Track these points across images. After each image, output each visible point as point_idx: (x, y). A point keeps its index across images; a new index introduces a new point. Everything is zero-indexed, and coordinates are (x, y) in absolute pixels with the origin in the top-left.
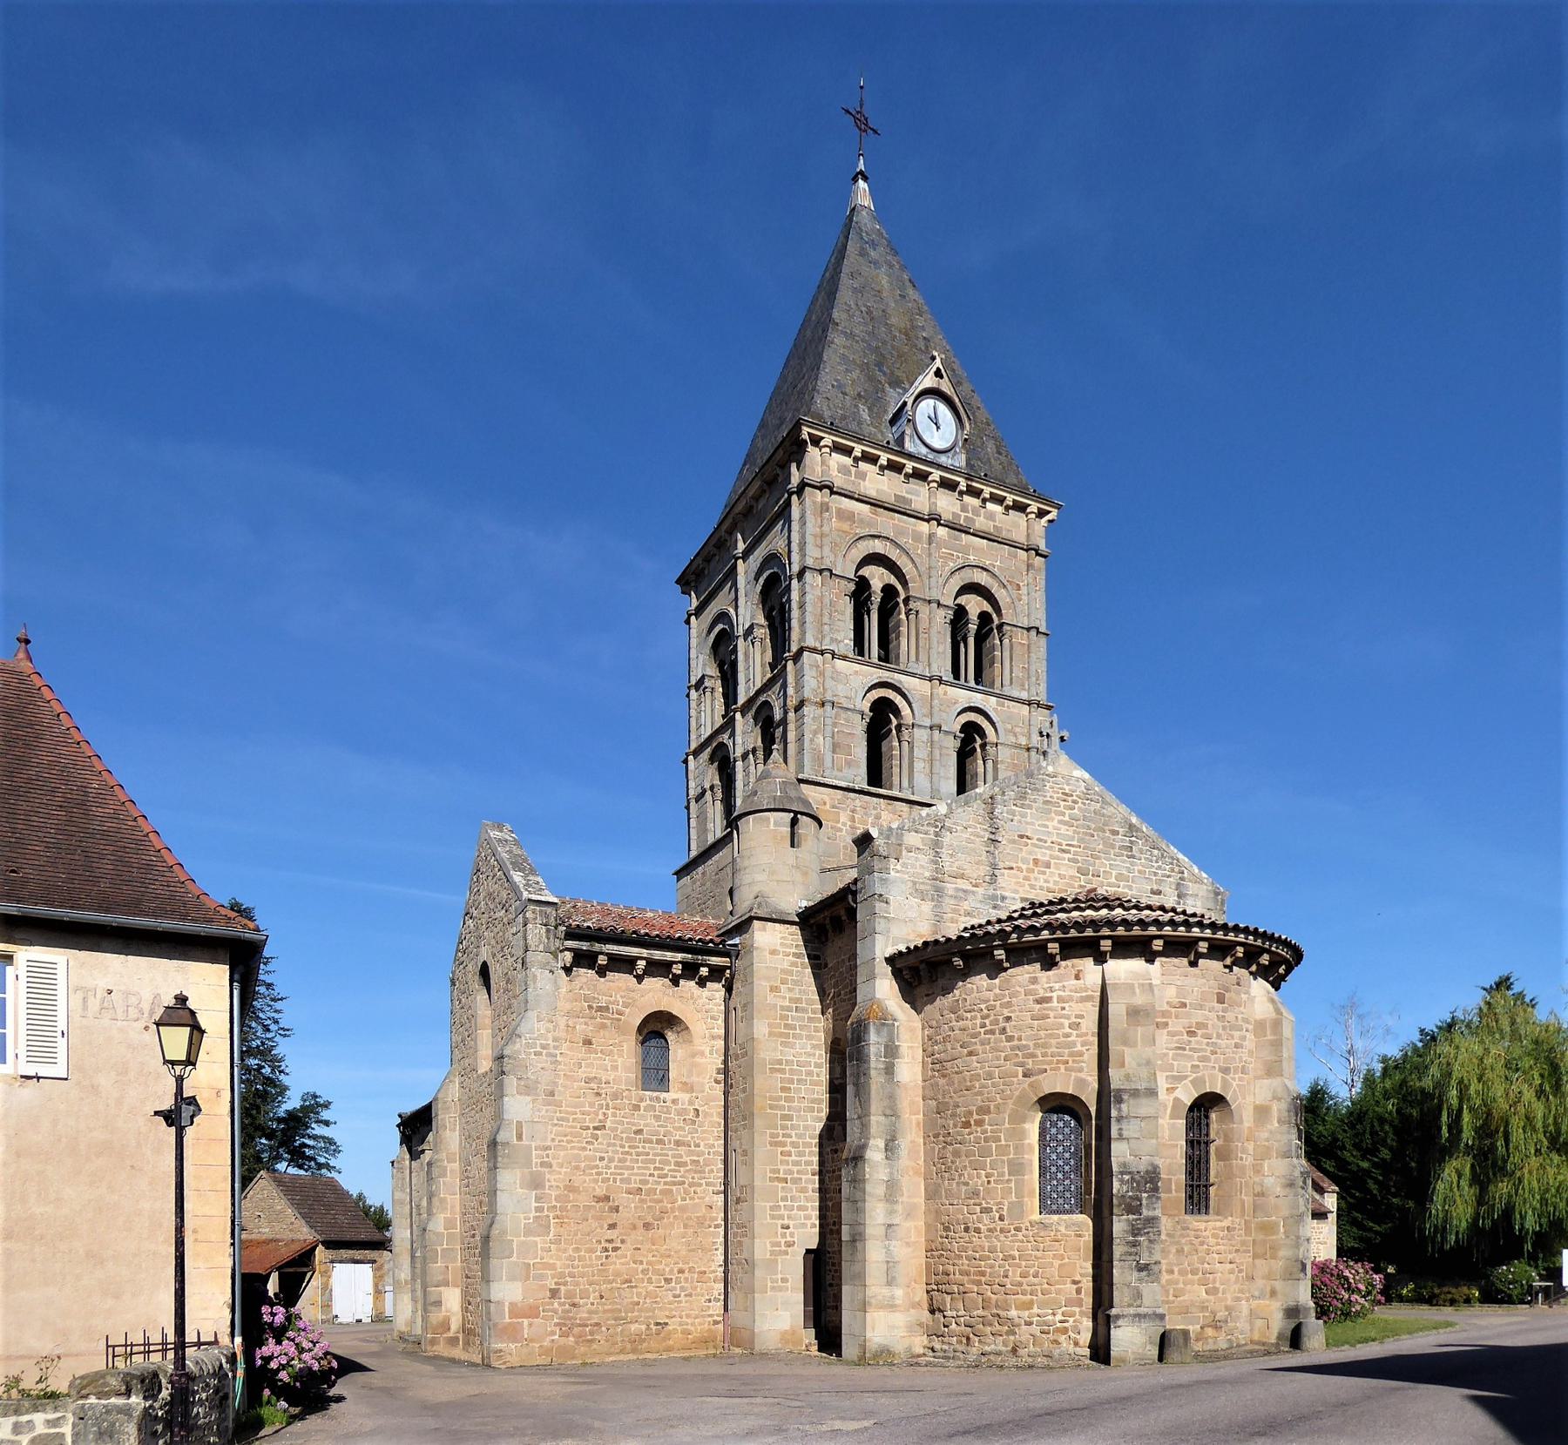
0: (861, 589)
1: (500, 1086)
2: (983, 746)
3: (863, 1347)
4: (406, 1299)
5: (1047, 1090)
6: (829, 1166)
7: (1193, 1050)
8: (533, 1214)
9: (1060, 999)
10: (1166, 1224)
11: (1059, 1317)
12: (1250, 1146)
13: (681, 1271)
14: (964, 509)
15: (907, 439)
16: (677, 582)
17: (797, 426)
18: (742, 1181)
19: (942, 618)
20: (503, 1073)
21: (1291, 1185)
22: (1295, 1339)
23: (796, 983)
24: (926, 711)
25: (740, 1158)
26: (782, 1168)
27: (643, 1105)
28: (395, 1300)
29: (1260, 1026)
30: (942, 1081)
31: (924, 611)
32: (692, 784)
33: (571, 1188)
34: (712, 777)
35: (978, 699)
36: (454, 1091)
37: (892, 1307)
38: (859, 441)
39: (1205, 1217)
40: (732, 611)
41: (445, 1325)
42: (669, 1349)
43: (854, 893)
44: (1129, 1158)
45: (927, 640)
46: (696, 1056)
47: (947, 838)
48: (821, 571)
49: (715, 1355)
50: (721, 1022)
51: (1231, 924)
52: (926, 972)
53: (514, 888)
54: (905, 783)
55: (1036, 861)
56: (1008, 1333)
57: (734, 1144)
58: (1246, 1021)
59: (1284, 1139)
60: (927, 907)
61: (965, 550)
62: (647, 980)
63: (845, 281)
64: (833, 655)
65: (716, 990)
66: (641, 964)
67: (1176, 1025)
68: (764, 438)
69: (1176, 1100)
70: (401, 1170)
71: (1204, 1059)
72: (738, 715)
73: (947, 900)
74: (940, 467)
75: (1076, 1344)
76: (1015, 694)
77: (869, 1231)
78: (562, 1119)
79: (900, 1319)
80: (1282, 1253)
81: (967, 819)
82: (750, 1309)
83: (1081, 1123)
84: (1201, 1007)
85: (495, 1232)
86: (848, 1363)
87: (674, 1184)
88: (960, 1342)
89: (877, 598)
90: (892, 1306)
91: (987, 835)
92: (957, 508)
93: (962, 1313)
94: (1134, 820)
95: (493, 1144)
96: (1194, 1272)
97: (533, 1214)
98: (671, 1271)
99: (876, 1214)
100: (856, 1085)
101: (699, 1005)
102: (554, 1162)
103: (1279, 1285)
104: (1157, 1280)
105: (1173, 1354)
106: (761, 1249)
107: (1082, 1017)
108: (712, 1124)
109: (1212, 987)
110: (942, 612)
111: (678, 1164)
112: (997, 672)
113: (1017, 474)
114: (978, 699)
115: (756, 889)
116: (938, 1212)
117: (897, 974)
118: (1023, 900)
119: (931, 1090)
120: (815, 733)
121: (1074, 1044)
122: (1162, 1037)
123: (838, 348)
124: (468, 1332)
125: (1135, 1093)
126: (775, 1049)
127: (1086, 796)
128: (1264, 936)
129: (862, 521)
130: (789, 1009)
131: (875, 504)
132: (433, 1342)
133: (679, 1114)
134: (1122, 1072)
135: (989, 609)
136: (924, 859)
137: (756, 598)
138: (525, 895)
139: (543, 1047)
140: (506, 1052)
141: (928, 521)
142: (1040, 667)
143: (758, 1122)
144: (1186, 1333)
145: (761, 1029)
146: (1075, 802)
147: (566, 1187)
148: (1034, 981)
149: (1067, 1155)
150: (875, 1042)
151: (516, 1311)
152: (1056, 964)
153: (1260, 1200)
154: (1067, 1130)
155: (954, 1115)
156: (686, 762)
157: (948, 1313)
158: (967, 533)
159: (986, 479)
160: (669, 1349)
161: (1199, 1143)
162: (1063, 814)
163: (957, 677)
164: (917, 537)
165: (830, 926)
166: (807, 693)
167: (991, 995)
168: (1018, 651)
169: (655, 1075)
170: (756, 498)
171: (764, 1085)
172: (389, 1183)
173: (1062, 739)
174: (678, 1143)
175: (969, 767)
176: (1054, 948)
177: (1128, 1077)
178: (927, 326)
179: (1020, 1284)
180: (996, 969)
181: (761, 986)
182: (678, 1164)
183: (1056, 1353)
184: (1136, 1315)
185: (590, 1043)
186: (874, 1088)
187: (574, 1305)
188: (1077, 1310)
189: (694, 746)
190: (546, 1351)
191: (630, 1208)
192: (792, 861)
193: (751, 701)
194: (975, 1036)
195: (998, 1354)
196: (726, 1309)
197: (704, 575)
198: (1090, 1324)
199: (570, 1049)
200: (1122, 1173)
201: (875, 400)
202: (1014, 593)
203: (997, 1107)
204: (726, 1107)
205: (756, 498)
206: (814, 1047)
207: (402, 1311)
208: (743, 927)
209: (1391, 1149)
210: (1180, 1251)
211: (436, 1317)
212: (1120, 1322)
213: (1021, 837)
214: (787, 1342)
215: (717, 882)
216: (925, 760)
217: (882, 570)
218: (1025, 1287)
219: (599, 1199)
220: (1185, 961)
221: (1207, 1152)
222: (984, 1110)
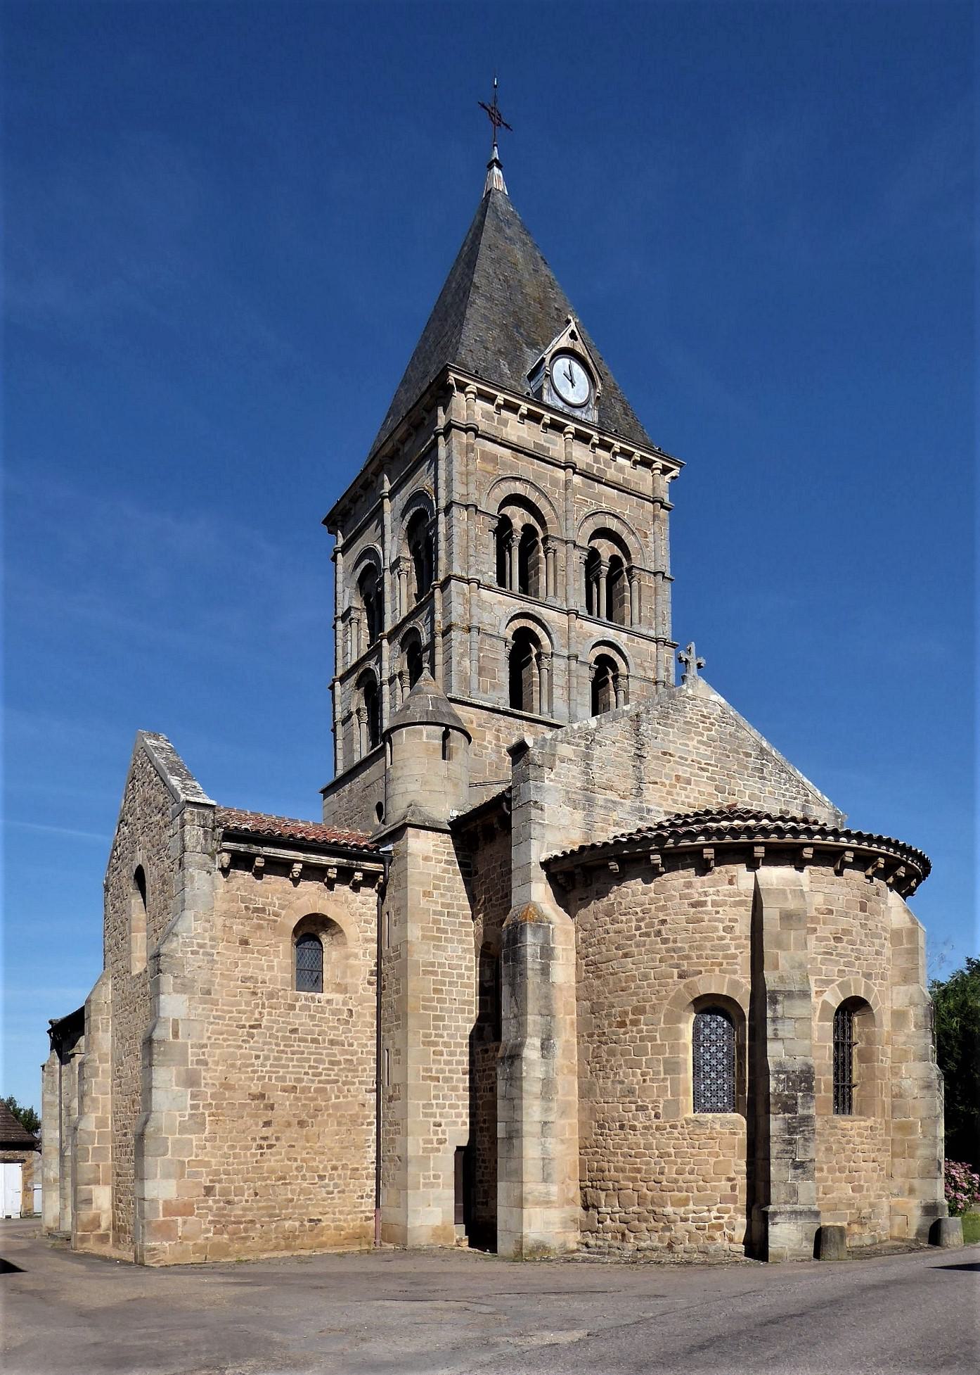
0: (504, 525)
1: (156, 984)
2: (615, 678)
3: (520, 1243)
4: (55, 1195)
5: (703, 991)
6: (479, 1066)
8: (189, 1111)
9: (714, 904)
10: (818, 1123)
11: (714, 1214)
12: (889, 1049)
13: (334, 1168)
14: (597, 460)
15: (545, 392)
16: (31, 1110)
17: (445, 372)
18: (395, 1080)
19: (577, 559)
20: (160, 971)
21: (928, 1087)
22: (934, 1235)
23: (448, 889)
24: (564, 642)
25: (393, 1057)
26: (434, 1067)
27: (298, 1004)
28: (44, 1197)
29: (896, 936)
30: (596, 983)
31: (562, 550)
32: (338, 708)
34: (358, 701)
35: (610, 634)
36: (107, 994)
37: (547, 1203)
38: (502, 390)
39: (850, 1117)
40: (379, 547)
41: (96, 1223)
42: (322, 1245)
43: (509, 801)
44: (784, 1058)
45: (564, 577)
46: (351, 958)
47: (597, 752)
48: (467, 507)
49: (368, 1252)
50: (374, 926)
51: (876, 836)
52: (580, 876)
53: (172, 792)
54: (545, 709)
55: (678, 778)
56: (663, 1229)
57: (387, 1043)
58: (884, 929)
59: (922, 1042)
60: (579, 815)
61: (598, 497)
62: (302, 884)
63: (484, 254)
64: (479, 584)
65: (369, 895)
66: (298, 867)
67: (824, 930)
68: (407, 391)
69: (825, 1003)
70: (51, 1074)
71: (848, 964)
72: (385, 642)
73: (598, 810)
74: (575, 420)
75: (731, 1240)
76: (644, 631)
77: (526, 1128)
79: (555, 1215)
80: (921, 1152)
81: (613, 735)
82: (403, 1205)
83: (738, 1026)
84: (847, 915)
85: (150, 1129)
86: (504, 1259)
87: (328, 1082)
88: (614, 1238)
89: (518, 536)
90: (548, 1202)
91: (634, 751)
92: (590, 459)
93: (617, 1209)
94: (765, 744)
95: (149, 1042)
96: (841, 1170)
97: (189, 1111)
98: (325, 1169)
99: (533, 1112)
100: (512, 985)
101: (353, 909)
102: (210, 1060)
103: (917, 1183)
104: (812, 1178)
105: (830, 1251)
106: (414, 1146)
107: (736, 921)
108: (365, 1024)
110: (577, 553)
111: (332, 1063)
112: (627, 611)
113: (643, 435)
114: (610, 634)
115: (409, 799)
116: (593, 1111)
117: (552, 879)
118: (667, 813)
119: (585, 992)
120: (462, 656)
121: (727, 947)
122: (812, 941)
123: (478, 308)
124: (118, 1229)
125: (789, 995)
126: (428, 952)
127: (722, 718)
128: (904, 849)
129: (504, 464)
131: (517, 449)
132: (83, 1239)
133: (334, 1013)
134: (777, 974)
135: (620, 554)
136: (576, 770)
137: (403, 534)
138: (183, 797)
139: (201, 946)
140: (163, 950)
141: (564, 468)
142: (666, 609)
143: (411, 1022)
144: (841, 1229)
145: (414, 932)
146: (712, 724)
147: (222, 1085)
148: (689, 885)
149: (720, 1055)
150: (531, 942)
151: (170, 1209)
152: (710, 869)
153: (898, 1101)
154: (720, 1031)
155: (608, 1015)
156: (332, 688)
157: (603, 1209)
159: (616, 435)
160: (322, 1245)
161: (843, 1045)
162: (702, 735)
163: (590, 613)
164: (554, 482)
165: (484, 836)
166: (455, 618)
167: (646, 899)
168: (645, 592)
169: (309, 976)
171: (417, 985)
172: (38, 1086)
173: (699, 666)
174: (332, 1042)
175: (602, 698)
176: (709, 853)
177: (782, 979)
178: (558, 299)
179: (676, 1181)
180: (651, 874)
181: (415, 891)
182: (332, 1063)
183: (712, 1249)
184: (794, 1212)
186: (530, 987)
187: (229, 1202)
188: (732, 1206)
189: (340, 672)
190: (200, 1249)
191: (285, 1106)
192: (444, 773)
193: (397, 629)
194: (630, 938)
195: (654, 1250)
196: (378, 1205)
197: (351, 514)
198: (745, 1221)
199: (227, 948)
200: (778, 1072)
201: (516, 361)
202: (642, 541)
203: (653, 1007)
204: (379, 1007)
206: (464, 950)
207: (51, 1207)
208: (397, 834)
209: (957, 1062)
210: (829, 1149)
211: (86, 1214)
212: (777, 1219)
213: (665, 754)
214: (439, 1237)
215: (364, 799)
216: (563, 686)
217: (522, 511)
218: (681, 1184)
219: (254, 1097)
220: (831, 870)
221: (850, 1054)
222: (639, 1010)
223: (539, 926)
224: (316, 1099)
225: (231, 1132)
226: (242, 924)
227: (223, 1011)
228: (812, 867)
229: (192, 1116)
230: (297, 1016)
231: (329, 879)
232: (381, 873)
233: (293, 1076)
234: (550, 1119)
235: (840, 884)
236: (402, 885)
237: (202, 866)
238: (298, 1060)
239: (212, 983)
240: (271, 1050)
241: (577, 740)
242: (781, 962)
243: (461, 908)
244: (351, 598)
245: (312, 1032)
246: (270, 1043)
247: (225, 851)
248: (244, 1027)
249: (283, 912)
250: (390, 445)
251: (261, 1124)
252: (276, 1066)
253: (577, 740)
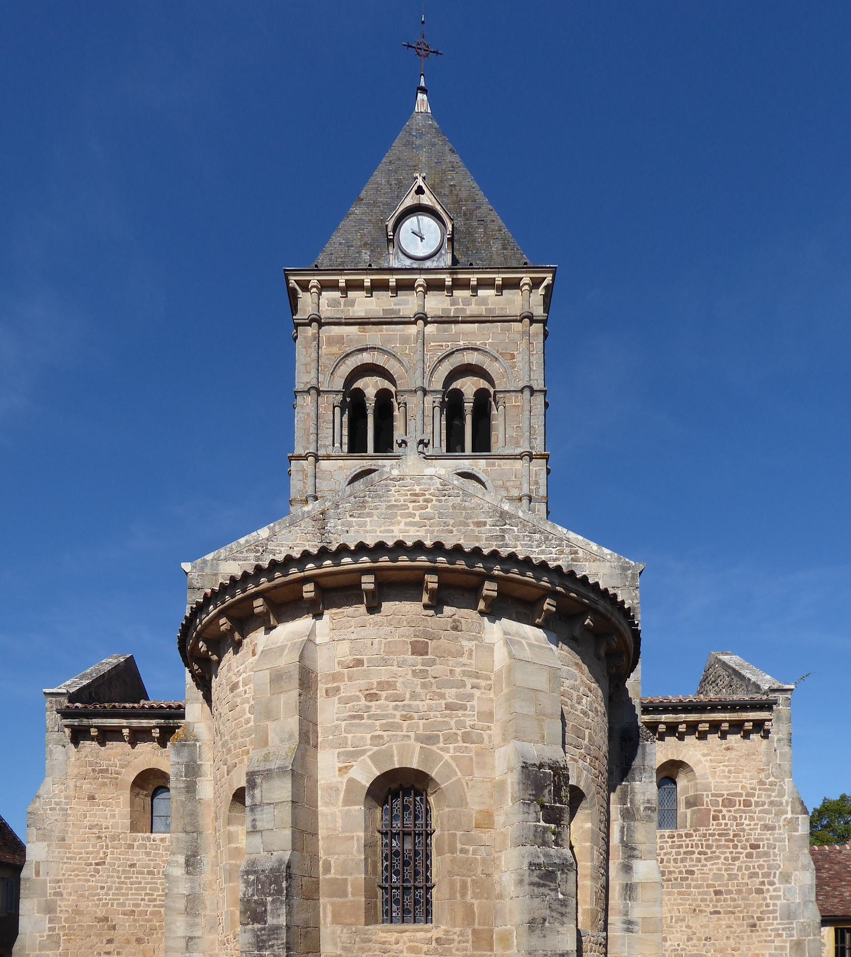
7: (376, 717)
27: (136, 844)
33: (77, 912)
38: (341, 271)
39: (429, 925)
67: (349, 689)
69: (351, 781)
78: (71, 858)
84: (385, 662)
102: (64, 892)
109: (405, 634)
131: (362, 323)
139: (57, 804)
146: (426, 501)
159: (471, 268)
164: (405, 340)
185: (94, 798)
191: (125, 927)
199: (77, 804)
219: (100, 920)
223: (184, 745)
224: (151, 920)
225: (80, 948)
227: (74, 853)
228: (334, 611)
229: (49, 936)
230: (136, 854)
233: (131, 902)
234: (198, 934)
235: (376, 624)
237: (57, 743)
238: (136, 889)
239: (66, 832)
240: (114, 882)
241: (245, 554)
242: (271, 735)
245: (148, 866)
246: (112, 876)
248: (91, 864)
249: (124, 770)
251: (105, 941)
252: (118, 895)
253: (245, 554)
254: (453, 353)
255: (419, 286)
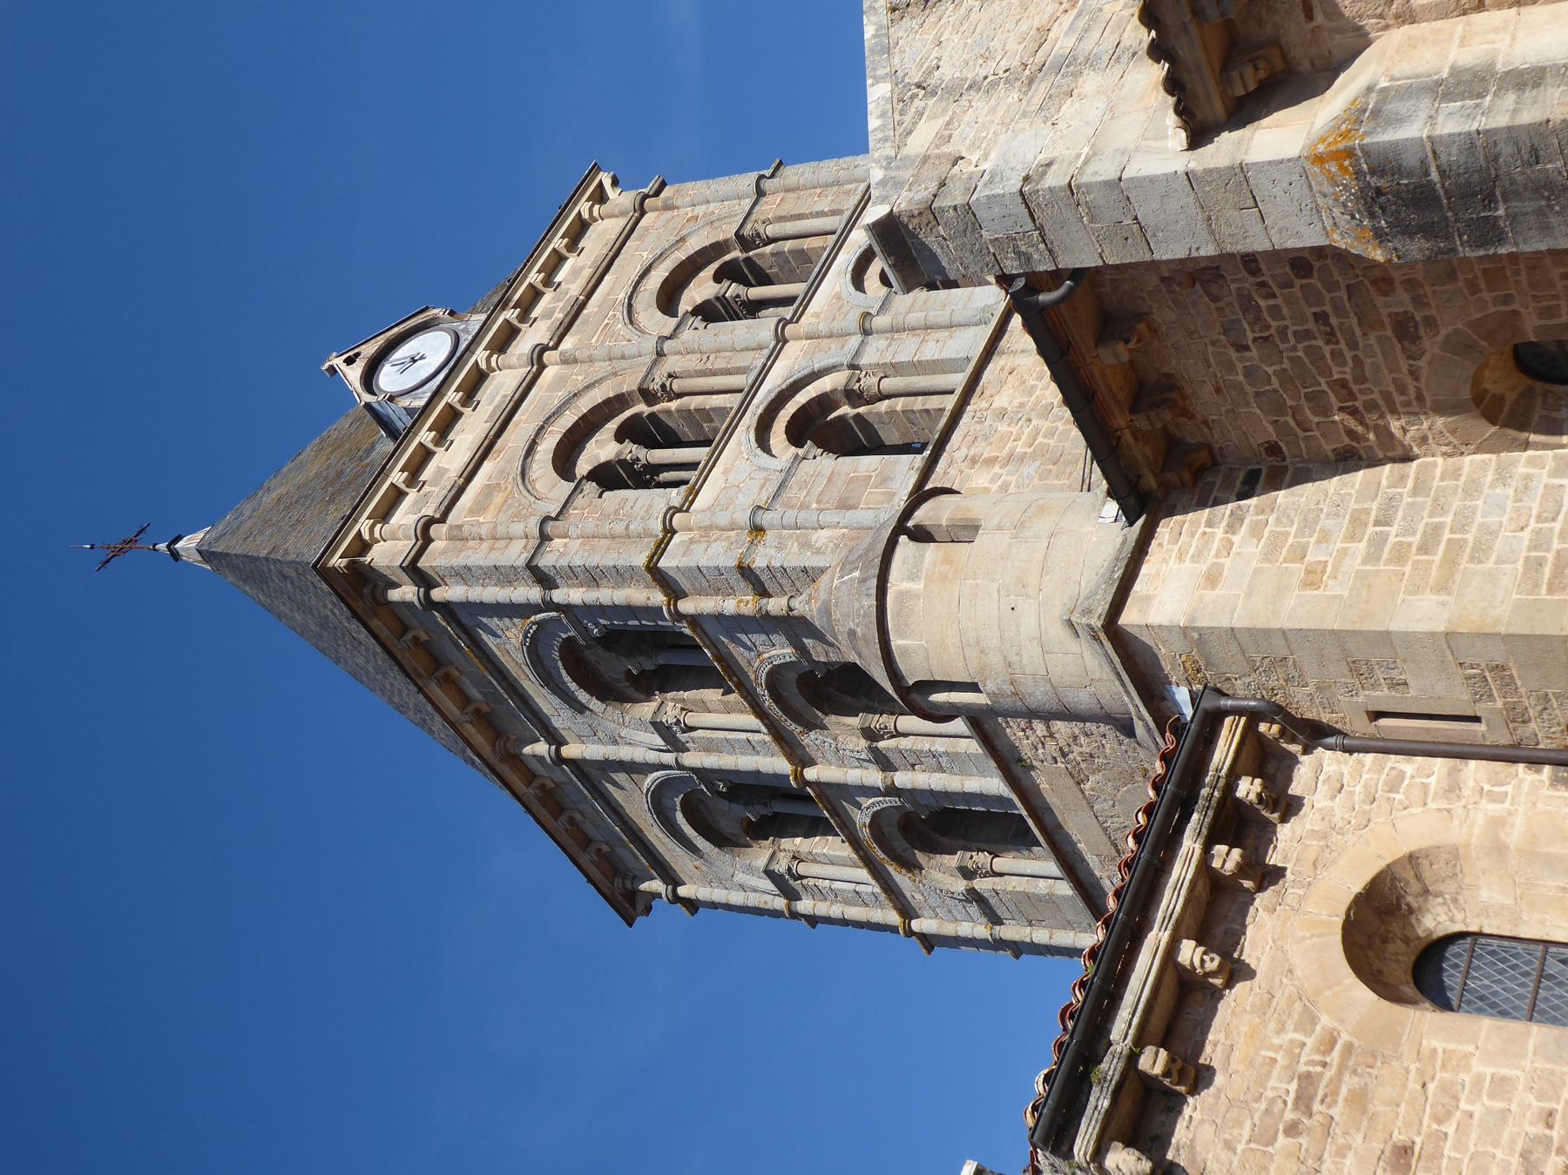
17: (321, 570)
19: (698, 335)
23: (1307, 525)
31: (673, 363)
32: (965, 929)
34: (942, 872)
38: (383, 471)
48: (545, 538)
50: (1409, 766)
65: (1317, 774)
74: (470, 348)
101: (1346, 820)
115: (1058, 632)
117: (1244, 112)
120: (806, 545)
129: (501, 472)
130: (1379, 541)
136: (979, 108)
150: (1413, 129)
158: (583, 305)
164: (559, 382)
170: (465, 700)
181: (1296, 610)
185: (1405, 1151)
189: (893, 918)
205: (465, 700)
208: (1135, 660)
226: (1341, 1153)
231: (1243, 870)
232: (1251, 728)
236: (1270, 648)
243: (1373, 490)
244: (750, 870)
247: (1099, 1153)
249: (1325, 1021)
250: (470, 730)
253: (908, 118)
254: (630, 306)
255: (488, 359)
